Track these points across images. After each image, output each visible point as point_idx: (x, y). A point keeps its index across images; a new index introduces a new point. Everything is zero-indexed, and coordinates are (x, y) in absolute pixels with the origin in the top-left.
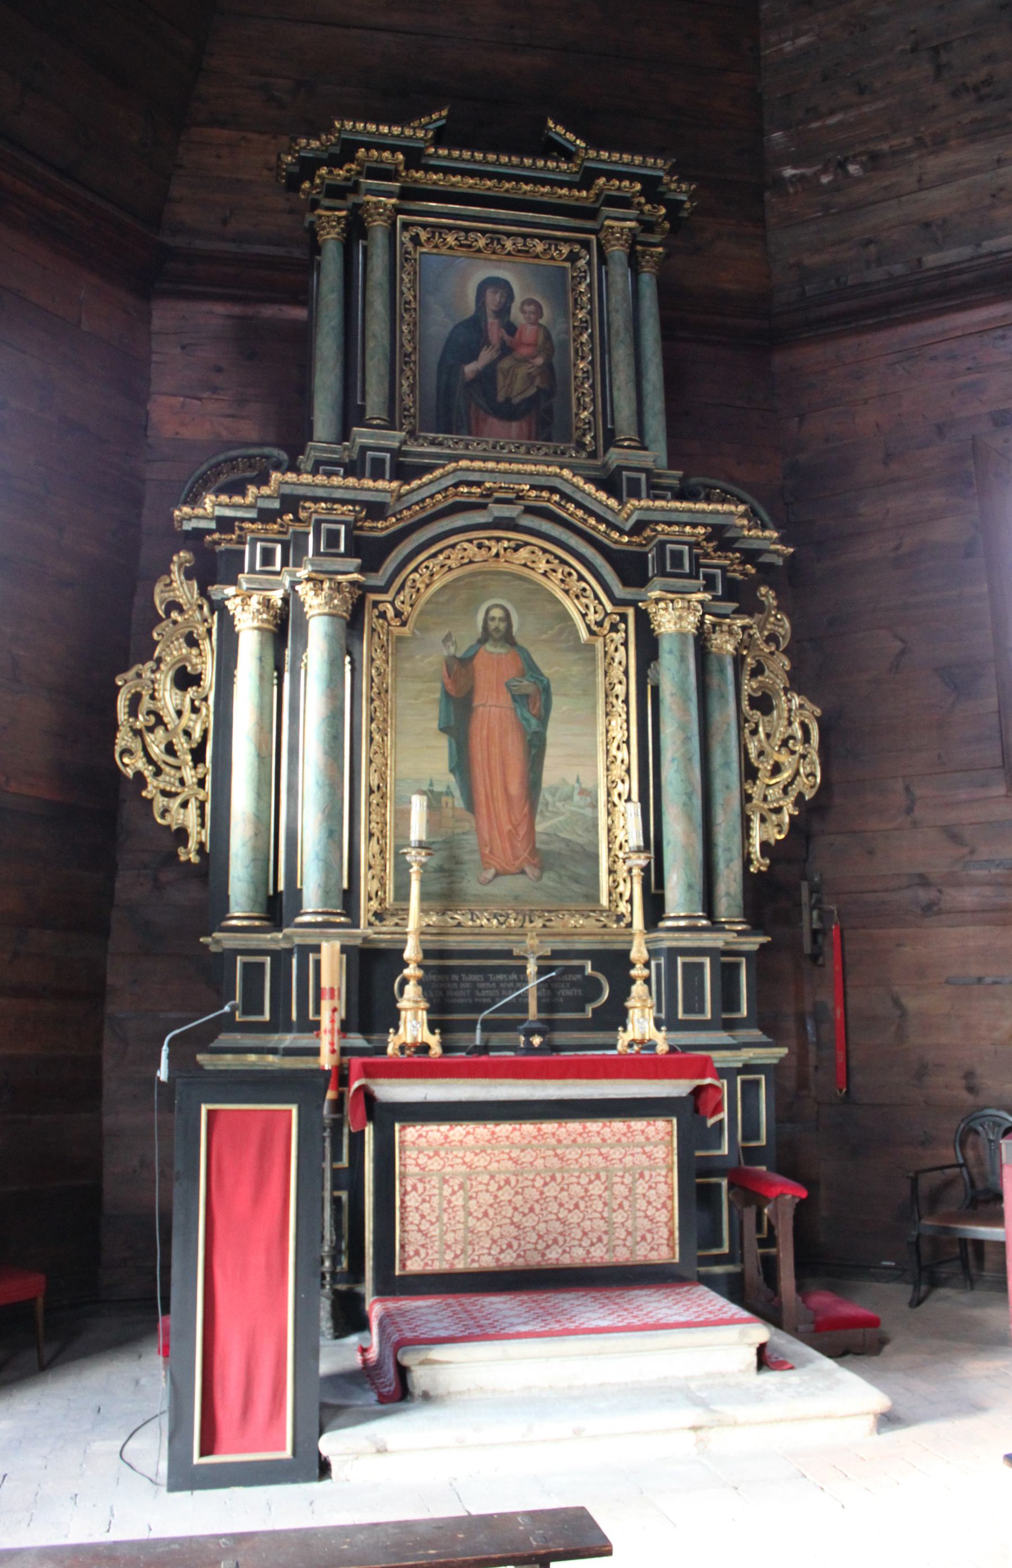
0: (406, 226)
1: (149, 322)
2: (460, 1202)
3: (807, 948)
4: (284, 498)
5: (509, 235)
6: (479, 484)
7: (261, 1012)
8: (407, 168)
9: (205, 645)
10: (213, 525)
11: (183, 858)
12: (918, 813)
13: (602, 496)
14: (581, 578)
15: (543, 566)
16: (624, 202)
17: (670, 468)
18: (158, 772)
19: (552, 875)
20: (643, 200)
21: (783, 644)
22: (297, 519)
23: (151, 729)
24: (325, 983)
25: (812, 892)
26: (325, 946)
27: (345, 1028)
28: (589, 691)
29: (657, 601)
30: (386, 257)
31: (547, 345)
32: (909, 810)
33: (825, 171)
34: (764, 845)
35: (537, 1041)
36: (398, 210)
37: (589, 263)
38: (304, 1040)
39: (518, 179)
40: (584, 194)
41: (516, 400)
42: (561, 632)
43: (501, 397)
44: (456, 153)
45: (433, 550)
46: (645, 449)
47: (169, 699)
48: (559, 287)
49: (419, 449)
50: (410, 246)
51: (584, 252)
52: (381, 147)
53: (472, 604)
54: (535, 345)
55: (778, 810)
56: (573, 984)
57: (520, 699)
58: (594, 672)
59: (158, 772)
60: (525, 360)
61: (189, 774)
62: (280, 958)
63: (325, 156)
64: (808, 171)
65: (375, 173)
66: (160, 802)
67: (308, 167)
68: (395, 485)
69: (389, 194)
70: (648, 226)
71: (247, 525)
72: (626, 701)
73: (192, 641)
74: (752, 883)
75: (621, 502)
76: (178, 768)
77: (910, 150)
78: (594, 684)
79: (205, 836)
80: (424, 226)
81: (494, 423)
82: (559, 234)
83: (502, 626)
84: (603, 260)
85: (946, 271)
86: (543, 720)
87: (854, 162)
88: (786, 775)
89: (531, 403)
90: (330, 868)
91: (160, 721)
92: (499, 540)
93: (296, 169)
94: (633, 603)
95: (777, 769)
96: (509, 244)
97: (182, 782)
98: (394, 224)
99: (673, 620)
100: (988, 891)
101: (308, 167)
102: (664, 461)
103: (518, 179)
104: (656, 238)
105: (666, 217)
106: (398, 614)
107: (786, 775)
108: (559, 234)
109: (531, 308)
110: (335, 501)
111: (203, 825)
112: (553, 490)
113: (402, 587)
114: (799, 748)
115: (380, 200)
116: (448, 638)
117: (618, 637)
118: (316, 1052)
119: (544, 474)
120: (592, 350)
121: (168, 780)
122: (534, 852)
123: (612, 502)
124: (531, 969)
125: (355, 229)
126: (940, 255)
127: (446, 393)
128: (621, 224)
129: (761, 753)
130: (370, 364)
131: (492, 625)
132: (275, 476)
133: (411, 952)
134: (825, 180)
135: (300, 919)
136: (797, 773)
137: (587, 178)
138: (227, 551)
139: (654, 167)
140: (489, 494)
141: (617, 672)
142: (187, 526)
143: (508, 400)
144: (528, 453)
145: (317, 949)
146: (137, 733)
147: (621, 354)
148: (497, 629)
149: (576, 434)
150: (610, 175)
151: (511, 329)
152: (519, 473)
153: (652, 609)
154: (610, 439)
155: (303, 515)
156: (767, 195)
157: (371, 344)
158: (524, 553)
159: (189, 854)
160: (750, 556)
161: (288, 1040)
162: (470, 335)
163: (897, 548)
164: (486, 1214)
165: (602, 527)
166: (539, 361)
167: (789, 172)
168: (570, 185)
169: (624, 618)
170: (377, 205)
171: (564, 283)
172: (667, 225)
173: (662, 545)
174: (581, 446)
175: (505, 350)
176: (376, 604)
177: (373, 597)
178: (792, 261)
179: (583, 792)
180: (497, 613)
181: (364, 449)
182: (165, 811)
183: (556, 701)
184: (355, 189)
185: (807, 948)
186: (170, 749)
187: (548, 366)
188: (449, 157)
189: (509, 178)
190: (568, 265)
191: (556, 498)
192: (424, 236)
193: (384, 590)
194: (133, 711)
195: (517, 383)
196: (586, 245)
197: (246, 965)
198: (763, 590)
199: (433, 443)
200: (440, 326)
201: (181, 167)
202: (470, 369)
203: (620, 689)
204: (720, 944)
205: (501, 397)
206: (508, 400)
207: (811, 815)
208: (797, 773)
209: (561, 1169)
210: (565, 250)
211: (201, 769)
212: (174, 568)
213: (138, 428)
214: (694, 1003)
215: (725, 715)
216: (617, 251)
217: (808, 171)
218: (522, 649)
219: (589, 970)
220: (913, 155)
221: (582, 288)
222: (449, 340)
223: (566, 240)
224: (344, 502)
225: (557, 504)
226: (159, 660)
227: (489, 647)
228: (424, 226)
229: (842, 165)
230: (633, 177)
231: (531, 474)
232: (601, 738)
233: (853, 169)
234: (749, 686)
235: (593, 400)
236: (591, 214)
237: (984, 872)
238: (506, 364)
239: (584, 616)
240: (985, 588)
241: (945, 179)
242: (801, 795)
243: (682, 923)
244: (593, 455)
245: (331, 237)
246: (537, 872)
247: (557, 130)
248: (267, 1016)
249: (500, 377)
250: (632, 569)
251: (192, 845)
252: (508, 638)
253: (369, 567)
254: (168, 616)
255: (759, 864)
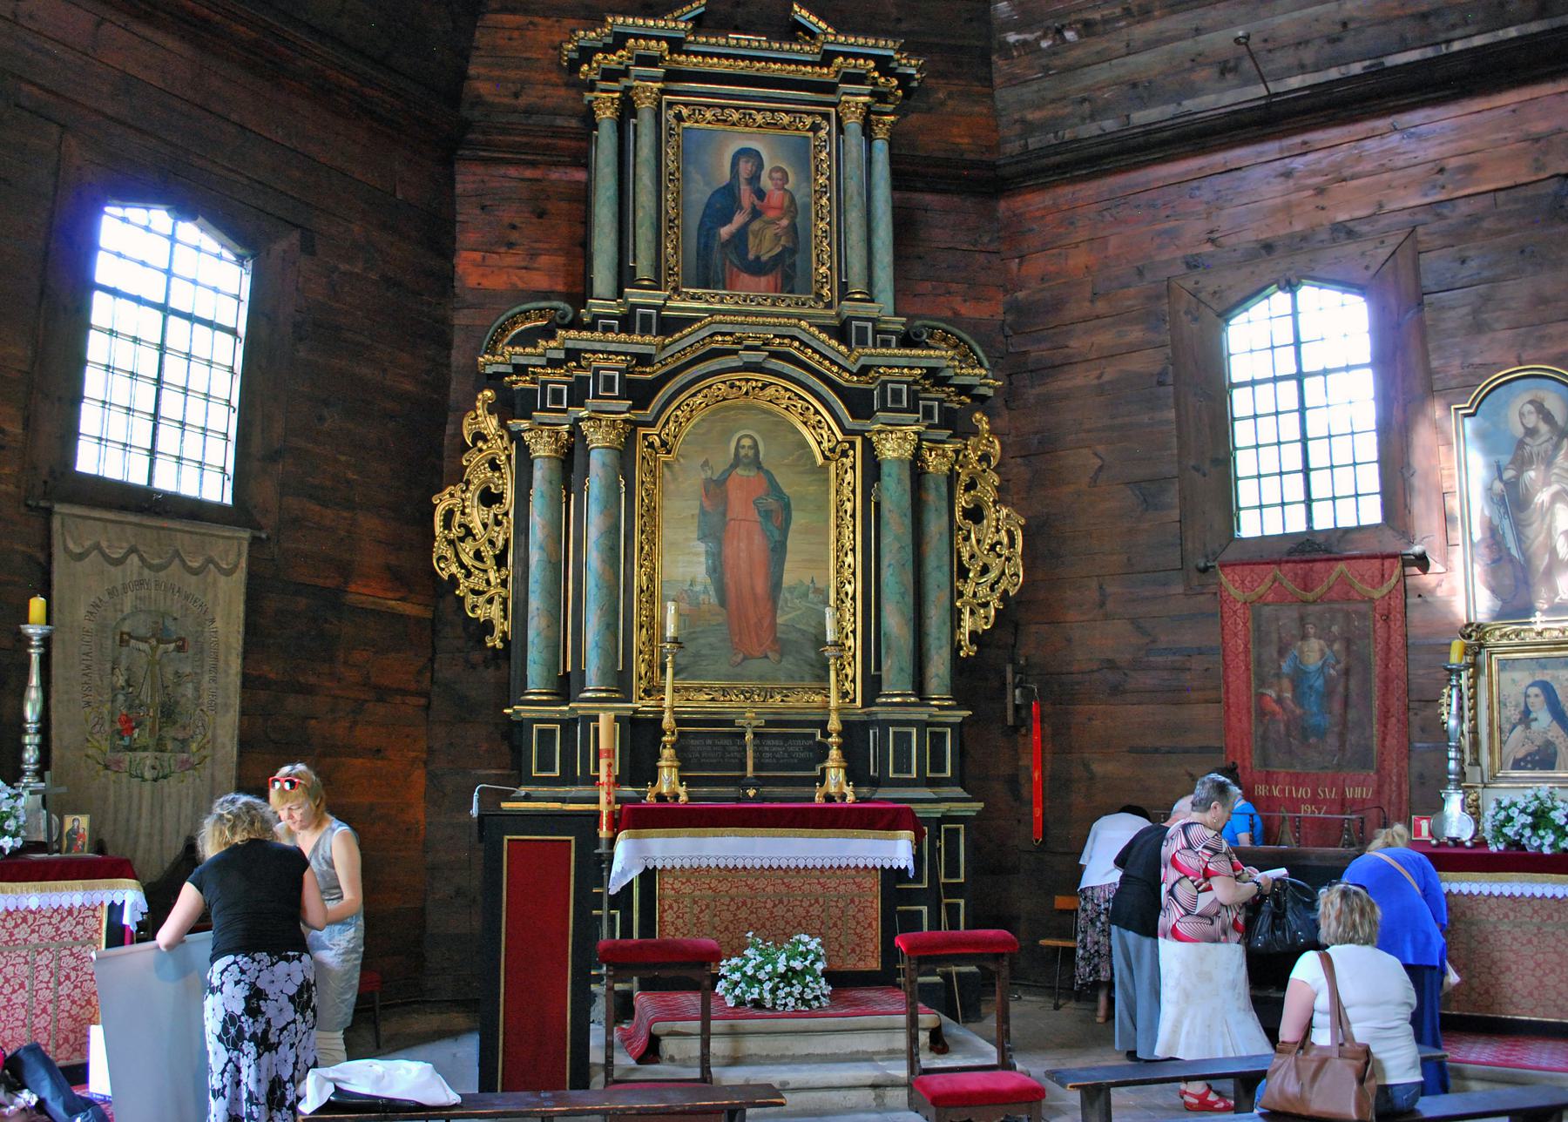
0: (670, 105)
1: (453, 188)
2: (707, 918)
3: (1010, 720)
4: (568, 351)
5: (759, 110)
6: (731, 334)
7: (553, 770)
8: (671, 53)
9: (506, 470)
10: (510, 369)
11: (490, 645)
12: (1109, 606)
13: (834, 343)
14: (817, 412)
15: (785, 402)
16: (858, 79)
17: (896, 315)
18: (469, 575)
19: (791, 659)
20: (876, 74)
21: (993, 463)
22: (580, 367)
23: (462, 539)
24: (602, 746)
25: (1015, 673)
26: (602, 716)
27: (619, 781)
28: (823, 507)
29: (879, 432)
30: (653, 137)
31: (792, 208)
32: (1102, 604)
33: (1044, 37)
34: (973, 634)
35: (751, 792)
36: (663, 92)
37: (829, 133)
38: (584, 791)
39: (767, 60)
40: (825, 70)
41: (764, 258)
42: (800, 457)
43: (751, 256)
44: (713, 40)
45: (693, 390)
46: (872, 301)
47: (477, 516)
48: (803, 155)
49: (682, 304)
50: (673, 122)
51: (825, 123)
52: (647, 38)
53: (727, 434)
54: (781, 208)
55: (985, 605)
56: (806, 748)
57: (767, 514)
58: (828, 492)
59: (469, 575)
60: (773, 222)
61: (492, 575)
62: (568, 725)
63: (600, 45)
64: (1029, 37)
65: (645, 61)
66: (470, 599)
67: (586, 54)
68: (659, 338)
69: (654, 79)
70: (880, 96)
71: (539, 370)
72: (853, 516)
73: (494, 466)
74: (959, 666)
75: (850, 349)
76: (485, 571)
77: (1118, 19)
78: (828, 501)
79: (507, 626)
80: (686, 105)
81: (745, 278)
82: (803, 107)
83: (751, 453)
84: (841, 129)
85: (1148, 130)
86: (784, 530)
87: (1071, 29)
88: (993, 575)
89: (777, 259)
90: (609, 654)
91: (469, 532)
92: (748, 380)
93: (575, 55)
94: (861, 433)
95: (985, 570)
96: (759, 118)
97: (488, 582)
98: (660, 104)
99: (892, 449)
100: (1165, 675)
101: (586, 54)
102: (891, 309)
103: (767, 60)
104: (890, 108)
105: (898, 87)
106: (664, 444)
107: (993, 575)
108: (803, 107)
109: (777, 175)
110: (610, 353)
111: (505, 618)
112: (793, 338)
113: (667, 422)
114: (1006, 552)
115: (647, 90)
116: (706, 463)
117: (848, 462)
118: (596, 800)
119: (785, 325)
120: (830, 212)
121: (476, 581)
122: (776, 640)
123: (842, 348)
124: (749, 737)
125: (627, 108)
126: (1146, 112)
127: (705, 250)
128: (856, 99)
129: (972, 556)
130: (639, 231)
131: (742, 452)
132: (561, 333)
133: (667, 721)
134: (1044, 44)
135: (583, 695)
136: (1003, 573)
137: (827, 58)
138: (522, 389)
139: (885, 48)
140: (739, 341)
141: (847, 491)
142: (489, 370)
143: (758, 258)
144: (774, 305)
145: (596, 718)
146: (451, 542)
147: (854, 217)
148: (746, 456)
149: (815, 287)
150: (846, 55)
151: (760, 194)
152: (764, 324)
153: (875, 438)
154: (844, 291)
155: (583, 363)
156: (994, 58)
157: (640, 214)
158: (771, 391)
159: (494, 641)
160: (964, 390)
161: (573, 791)
162: (724, 202)
163: (1099, 377)
164: (727, 928)
165: (835, 369)
166: (785, 222)
167: (1012, 38)
168: (813, 64)
169: (853, 445)
170: (644, 90)
171: (807, 152)
172: (900, 93)
173: (884, 383)
174: (819, 297)
175: (756, 214)
176: (645, 436)
177: (642, 431)
178: (1016, 116)
179: (817, 591)
180: (746, 442)
181: (635, 306)
182: (474, 607)
183: (794, 514)
184: (625, 73)
185: (1010, 720)
186: (478, 556)
187: (793, 227)
188: (707, 44)
189: (759, 59)
190: (811, 134)
191: (796, 344)
192: (685, 112)
193: (652, 424)
194: (447, 525)
195: (764, 245)
196: (826, 116)
197: (540, 731)
198: (978, 416)
199: (693, 297)
200: (700, 193)
201: (478, 48)
202: (725, 231)
203: (848, 506)
204: (925, 717)
205: (751, 256)
206: (758, 258)
207: (1012, 613)
208: (1003, 573)
209: (823, 895)
210: (808, 121)
211: (503, 572)
212: (479, 404)
213: (445, 281)
214: (938, 765)
215: (936, 525)
216: (853, 123)
217: (1029, 37)
218: (767, 472)
219: (819, 737)
220: (1122, 24)
221: (823, 155)
222: (708, 205)
223: (809, 113)
224: (617, 353)
225: (797, 349)
226: (468, 483)
227: (739, 471)
228: (686, 105)
229: (1059, 31)
230: (866, 57)
231: (774, 325)
232: (833, 546)
233: (1070, 35)
234: (963, 500)
235: (830, 257)
236: (830, 88)
237: (1159, 659)
238: (755, 226)
239: (820, 443)
240: (1172, 414)
241: (1150, 45)
242: (1006, 592)
243: (898, 699)
244: (829, 306)
245: (606, 114)
246: (777, 657)
247: (802, 14)
248: (557, 773)
249: (751, 238)
250: (859, 404)
251: (497, 633)
252: (756, 463)
253: (641, 402)
254: (475, 445)
255: (968, 650)
